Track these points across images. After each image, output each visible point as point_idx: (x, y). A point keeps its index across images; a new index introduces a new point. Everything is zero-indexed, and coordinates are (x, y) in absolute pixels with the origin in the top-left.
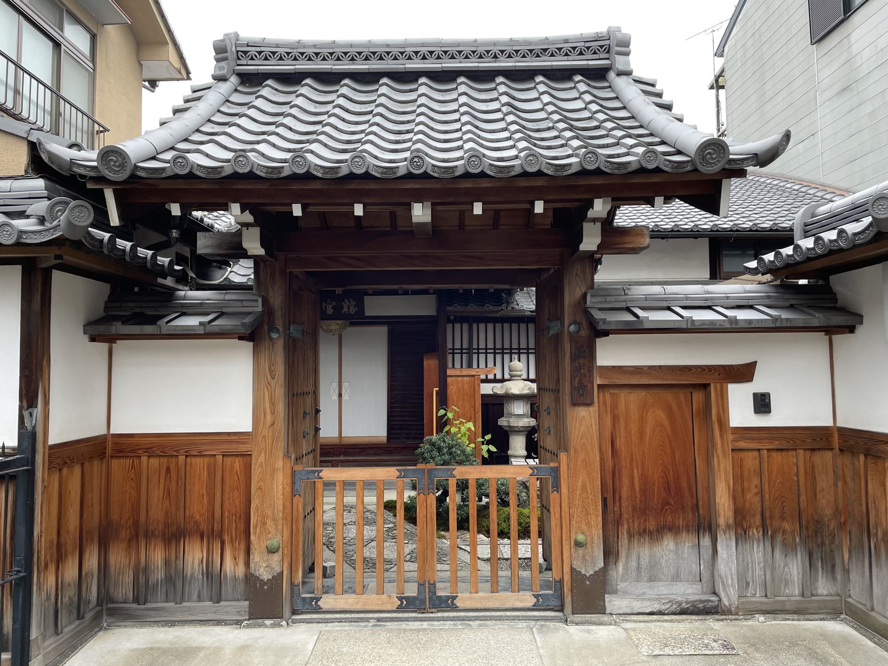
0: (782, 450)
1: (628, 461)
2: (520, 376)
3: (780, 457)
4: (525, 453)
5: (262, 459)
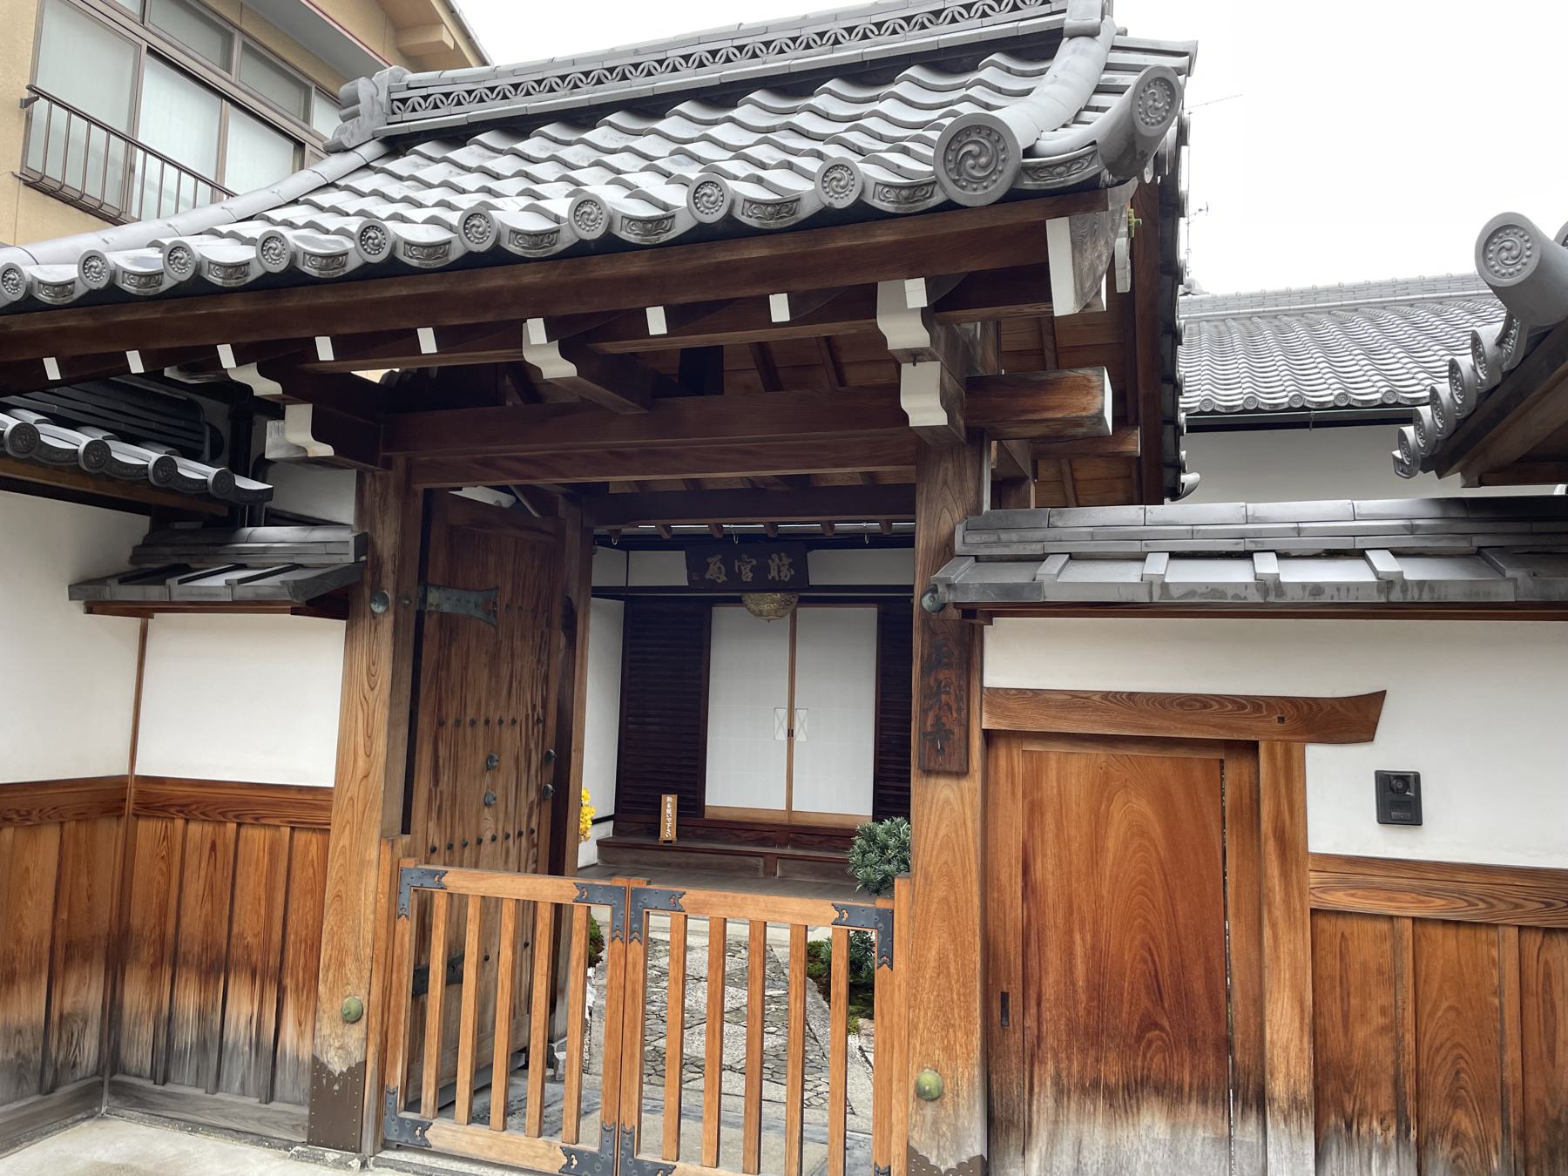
0: (1458, 923)
1: (1060, 914)
3: (1451, 943)
5: (345, 841)
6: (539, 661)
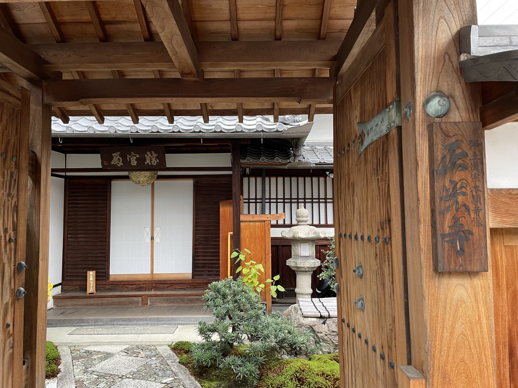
2: (306, 221)
4: (311, 291)
6: (9, 195)
